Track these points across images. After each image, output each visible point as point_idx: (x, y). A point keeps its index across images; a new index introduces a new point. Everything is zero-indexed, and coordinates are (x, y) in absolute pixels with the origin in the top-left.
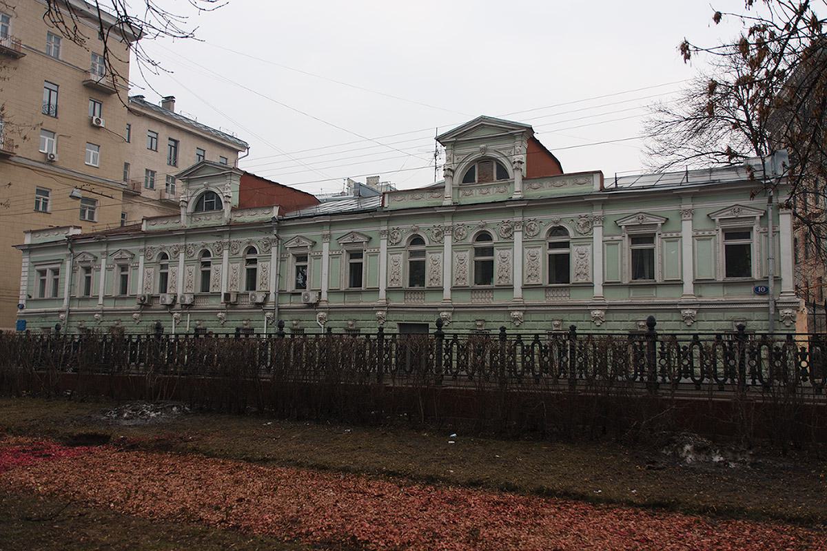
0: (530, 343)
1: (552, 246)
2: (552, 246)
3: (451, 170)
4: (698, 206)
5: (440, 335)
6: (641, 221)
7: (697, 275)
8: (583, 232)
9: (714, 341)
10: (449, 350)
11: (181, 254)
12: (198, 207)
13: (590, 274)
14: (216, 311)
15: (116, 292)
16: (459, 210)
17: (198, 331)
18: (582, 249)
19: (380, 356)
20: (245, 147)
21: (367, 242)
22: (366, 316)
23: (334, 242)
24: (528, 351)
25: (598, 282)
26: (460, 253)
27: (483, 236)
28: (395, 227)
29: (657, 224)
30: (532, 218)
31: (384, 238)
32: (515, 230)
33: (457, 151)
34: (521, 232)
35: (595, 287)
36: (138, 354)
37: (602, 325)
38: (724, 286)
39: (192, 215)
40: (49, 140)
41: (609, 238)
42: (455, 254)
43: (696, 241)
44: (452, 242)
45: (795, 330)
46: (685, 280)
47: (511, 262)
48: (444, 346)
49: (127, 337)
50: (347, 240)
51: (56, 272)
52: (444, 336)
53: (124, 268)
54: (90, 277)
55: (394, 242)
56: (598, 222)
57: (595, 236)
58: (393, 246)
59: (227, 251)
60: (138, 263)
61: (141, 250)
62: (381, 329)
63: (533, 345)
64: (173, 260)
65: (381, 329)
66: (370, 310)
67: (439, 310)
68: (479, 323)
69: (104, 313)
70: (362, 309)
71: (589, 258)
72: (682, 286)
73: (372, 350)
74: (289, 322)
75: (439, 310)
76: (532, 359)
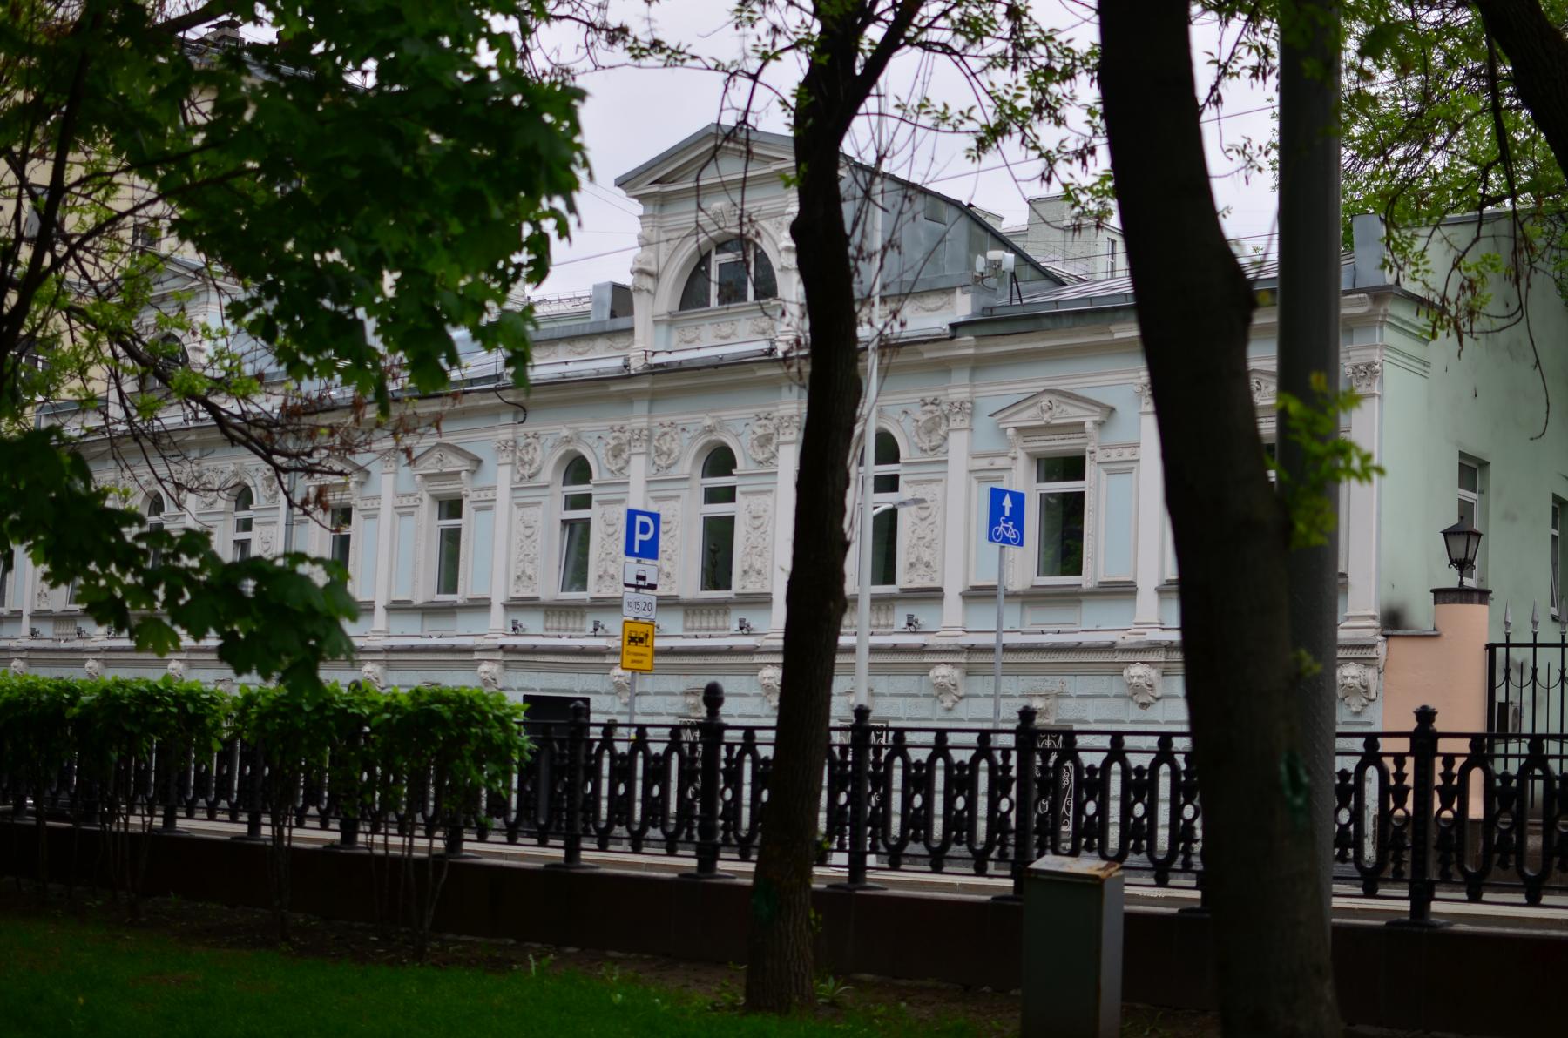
0: (1145, 761)
3: (650, 274)
4: (984, 391)
6: (1047, 416)
8: (926, 446)
11: (634, 459)
12: (692, 296)
14: (1120, 658)
15: (425, 589)
16: (669, 381)
17: (1027, 727)
21: (473, 473)
23: (983, 423)
25: (26, 612)
28: (667, 420)
29: (1082, 424)
30: (667, 420)
33: (670, 221)
34: (965, 434)
35: (946, 601)
37: (1367, 710)
39: (671, 321)
41: (984, 463)
42: (518, 513)
44: (513, 482)
45: (1370, 724)
47: (938, 520)
48: (723, 765)
49: (596, 733)
50: (1028, 417)
53: (452, 507)
55: (526, 471)
56: (959, 418)
57: (951, 457)
59: (642, 459)
60: (494, 488)
61: (502, 448)
64: (607, 478)
69: (973, 657)
70: (1027, 658)
76: (1080, 809)
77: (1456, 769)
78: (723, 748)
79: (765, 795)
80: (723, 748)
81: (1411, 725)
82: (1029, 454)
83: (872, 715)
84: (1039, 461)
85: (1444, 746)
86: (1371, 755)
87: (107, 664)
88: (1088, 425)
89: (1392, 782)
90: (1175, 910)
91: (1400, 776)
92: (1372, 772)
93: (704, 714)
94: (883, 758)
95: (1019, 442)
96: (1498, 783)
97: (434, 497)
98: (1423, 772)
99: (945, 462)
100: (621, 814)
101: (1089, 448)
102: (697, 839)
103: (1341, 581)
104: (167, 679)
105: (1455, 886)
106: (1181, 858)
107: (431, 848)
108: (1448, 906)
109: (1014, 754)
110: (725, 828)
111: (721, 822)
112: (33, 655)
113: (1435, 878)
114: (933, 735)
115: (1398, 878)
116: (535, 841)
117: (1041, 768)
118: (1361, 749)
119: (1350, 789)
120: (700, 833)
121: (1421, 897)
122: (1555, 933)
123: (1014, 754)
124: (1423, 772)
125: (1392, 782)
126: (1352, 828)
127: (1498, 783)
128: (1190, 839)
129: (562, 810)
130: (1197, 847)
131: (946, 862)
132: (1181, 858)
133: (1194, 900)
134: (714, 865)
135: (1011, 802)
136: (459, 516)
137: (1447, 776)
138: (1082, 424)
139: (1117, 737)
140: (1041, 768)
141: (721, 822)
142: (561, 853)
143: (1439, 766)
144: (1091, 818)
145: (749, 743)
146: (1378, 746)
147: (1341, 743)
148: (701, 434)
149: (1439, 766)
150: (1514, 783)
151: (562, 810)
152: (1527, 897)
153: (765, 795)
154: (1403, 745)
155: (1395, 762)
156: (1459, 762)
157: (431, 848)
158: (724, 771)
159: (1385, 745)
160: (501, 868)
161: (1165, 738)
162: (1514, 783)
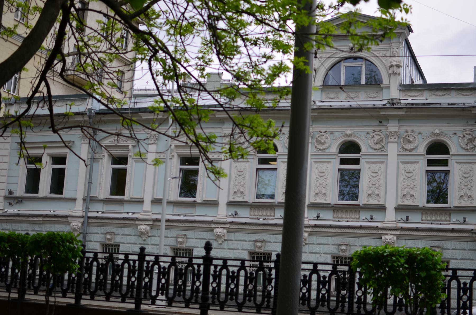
1: (343, 161)
2: (343, 161)
5: (208, 260)
7: (155, 194)
9: (256, 267)
10: (217, 277)
13: (382, 195)
18: (375, 167)
19: (140, 279)
20: (412, 32)
22: (126, 231)
24: (233, 277)
25: (391, 206)
26: (408, 165)
27: (351, 147)
29: (128, 146)
31: (393, 140)
32: (389, 140)
34: (396, 144)
35: (144, 203)
36: (10, 274)
38: (104, 203)
40: (17, 18)
42: (402, 166)
43: (134, 163)
46: (145, 200)
51: (61, 160)
52: (212, 262)
54: (62, 172)
58: (406, 153)
62: (142, 249)
63: (311, 275)
65: (142, 249)
66: (131, 222)
67: (137, 223)
68: (344, 247)
71: (382, 177)
72: (386, 211)
73: (131, 272)
74: (248, 243)
75: (137, 223)
76: (328, 291)
77: (150, 265)
78: (145, 263)
79: (3, 270)
80: (145, 263)
81: (138, 250)
82: (178, 155)
83: (146, 251)
84: (53, 158)
85: (148, 258)
86: (126, 260)
87: (399, 237)
88: (130, 147)
89: (196, 272)
90: (125, 310)
91: (199, 271)
92: (126, 265)
93: (205, 254)
94: (89, 262)
95: (175, 150)
96: (162, 270)
97: (179, 155)
98: (141, 265)
99: (387, 155)
100: (101, 286)
101: (129, 155)
102: (18, 287)
103: (448, 213)
104: (387, 244)
105: (216, 305)
106: (130, 293)
107: (9, 297)
108: (85, 302)
109: (137, 262)
110: (29, 283)
111: (143, 290)
112: (403, 233)
113: (83, 292)
114: (222, 261)
115: (131, 297)
116: (120, 300)
117: (86, 263)
118: (124, 258)
119: (307, 281)
120: (20, 285)
121: (138, 304)
122: (100, 308)
123: (137, 262)
124: (141, 265)
125: (196, 272)
126: (307, 294)
127: (162, 270)
128: (17, 279)
129: (28, 279)
130: (200, 295)
131: (126, 299)
132: (130, 293)
133: (43, 301)
134: (24, 296)
135: (272, 287)
136: (65, 164)
137: (215, 271)
138: (128, 146)
139: (315, 265)
140: (86, 263)
141: (27, 281)
142: (73, 301)
143: (145, 264)
144: (101, 280)
145: (95, 258)
146: (457, 273)
147: (304, 266)
148: (344, 136)
149: (145, 264)
150: (167, 270)
151: (28, 279)
152: (257, 310)
153: (3, 270)
154: (136, 257)
155: (133, 263)
156: (151, 263)
157: (9, 297)
158: (29, 264)
159: (131, 257)
160: (39, 303)
161: (243, 261)
162: (167, 270)
